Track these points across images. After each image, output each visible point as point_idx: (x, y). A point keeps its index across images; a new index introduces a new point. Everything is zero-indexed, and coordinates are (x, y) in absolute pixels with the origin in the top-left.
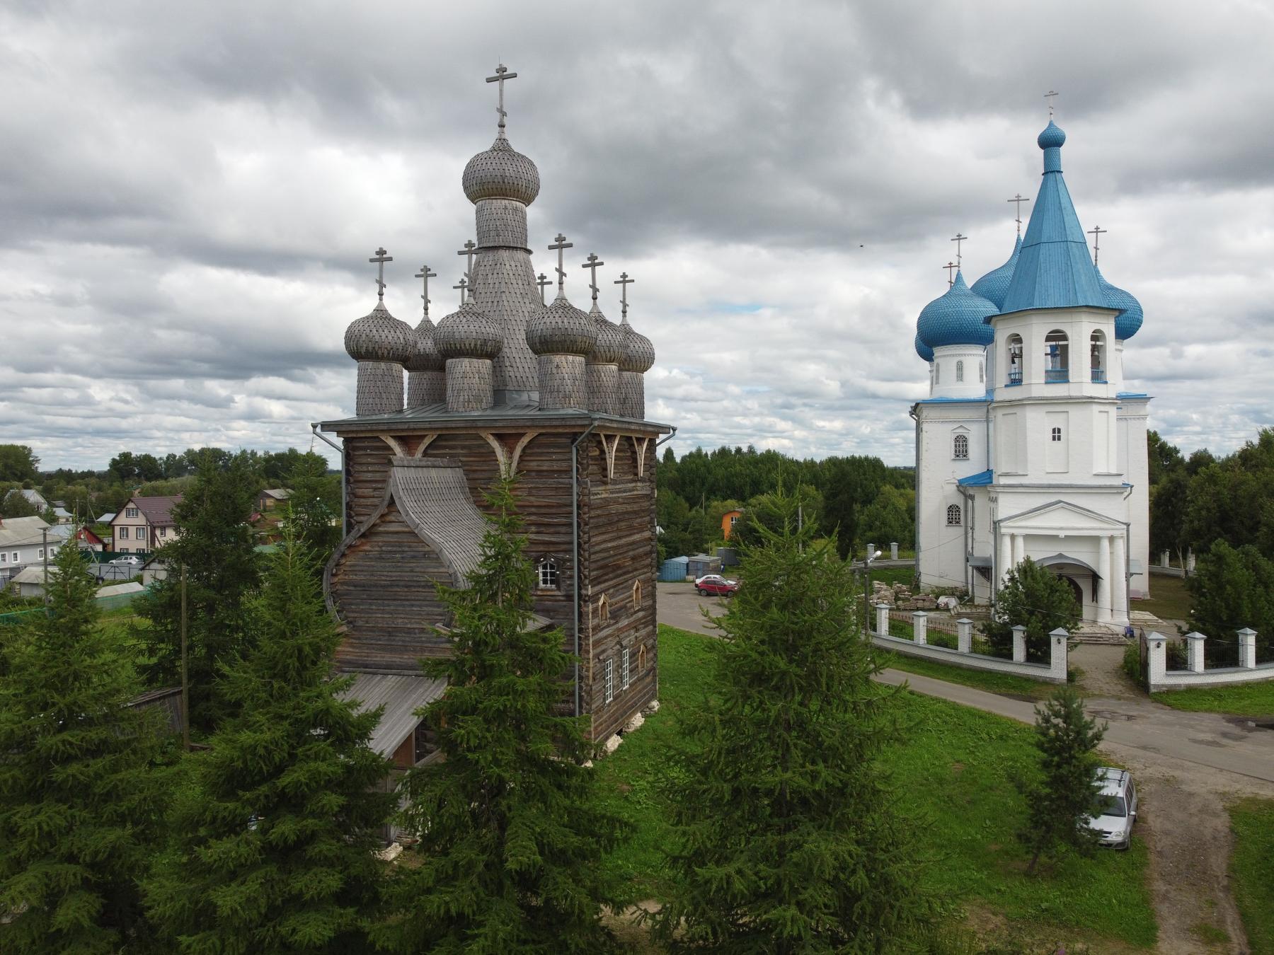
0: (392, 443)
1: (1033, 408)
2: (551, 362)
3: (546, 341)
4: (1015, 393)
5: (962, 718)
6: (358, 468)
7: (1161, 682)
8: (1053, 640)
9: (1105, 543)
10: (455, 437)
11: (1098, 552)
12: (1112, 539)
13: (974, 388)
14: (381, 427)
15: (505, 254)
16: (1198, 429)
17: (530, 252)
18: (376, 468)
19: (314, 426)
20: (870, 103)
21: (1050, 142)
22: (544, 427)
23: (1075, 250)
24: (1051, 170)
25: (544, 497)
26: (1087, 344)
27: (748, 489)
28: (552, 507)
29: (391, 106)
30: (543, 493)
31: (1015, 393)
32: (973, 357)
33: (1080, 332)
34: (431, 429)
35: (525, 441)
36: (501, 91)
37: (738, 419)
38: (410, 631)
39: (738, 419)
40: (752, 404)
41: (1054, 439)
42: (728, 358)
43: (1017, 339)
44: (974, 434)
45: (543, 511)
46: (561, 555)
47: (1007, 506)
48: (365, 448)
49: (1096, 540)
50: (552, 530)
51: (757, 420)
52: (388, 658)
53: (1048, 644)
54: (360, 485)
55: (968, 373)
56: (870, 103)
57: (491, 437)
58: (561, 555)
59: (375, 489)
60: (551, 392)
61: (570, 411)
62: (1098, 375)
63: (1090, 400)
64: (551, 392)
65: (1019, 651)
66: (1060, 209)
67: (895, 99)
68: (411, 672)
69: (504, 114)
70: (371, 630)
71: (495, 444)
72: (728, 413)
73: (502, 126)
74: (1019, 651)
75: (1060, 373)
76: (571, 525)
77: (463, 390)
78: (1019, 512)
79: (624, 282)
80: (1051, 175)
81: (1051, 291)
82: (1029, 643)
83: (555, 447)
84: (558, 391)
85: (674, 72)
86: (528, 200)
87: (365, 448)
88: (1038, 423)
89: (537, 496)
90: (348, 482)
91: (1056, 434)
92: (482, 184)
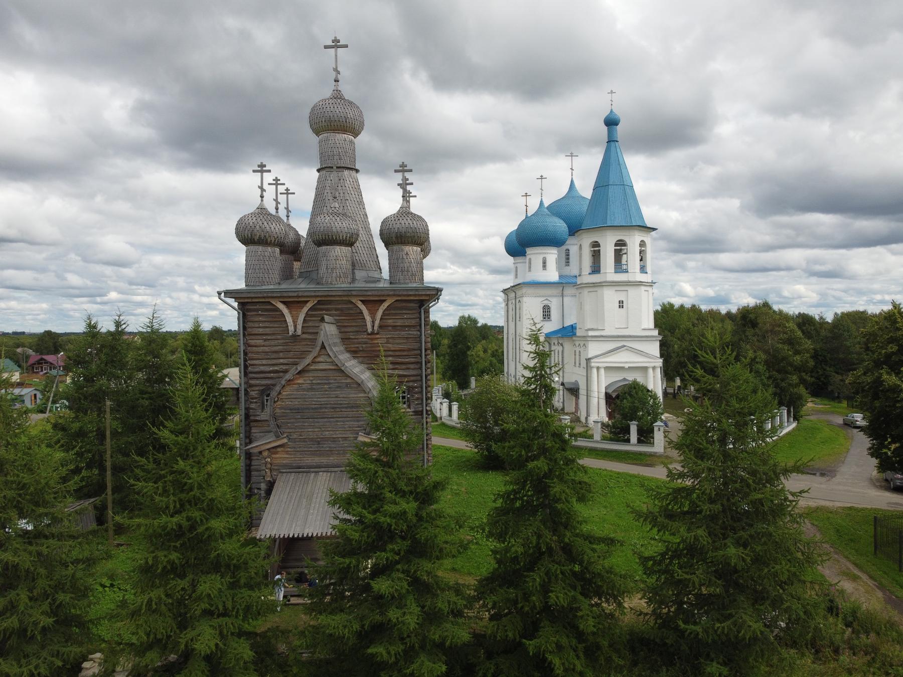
0: (281, 306)
2: (402, 250)
3: (401, 236)
4: (595, 278)
5: (628, 479)
6: (250, 324)
8: (656, 429)
9: (651, 371)
10: (330, 302)
11: (646, 377)
12: (654, 368)
13: (552, 275)
14: (275, 295)
15: (346, 172)
16: (27, 317)
17: (357, 171)
18: (267, 325)
19: (219, 293)
20: (407, 77)
22: (399, 296)
25: (398, 344)
26: (638, 249)
28: (404, 351)
29: (28, 34)
30: (397, 341)
31: (595, 278)
32: (552, 255)
33: (634, 240)
34: (388, 295)
35: (385, 305)
36: (336, 56)
38: (334, 440)
43: (596, 244)
44: (554, 304)
45: (397, 353)
46: (411, 384)
47: (594, 349)
48: (257, 310)
50: (404, 367)
52: (317, 460)
53: (652, 431)
54: (253, 337)
55: (546, 265)
56: (407, 77)
57: (360, 303)
58: (411, 384)
59: (265, 340)
60: (402, 271)
61: (415, 285)
62: (643, 269)
63: (640, 284)
64: (402, 271)
65: (634, 436)
66: (619, 164)
67: (423, 75)
68: (336, 469)
69: (339, 73)
70: (304, 440)
71: (363, 307)
73: (336, 81)
74: (634, 436)
75: (596, 269)
76: (421, 363)
77: (336, 268)
78: (600, 353)
79: (287, 194)
80: (612, 143)
81: (616, 217)
82: (640, 432)
83: (405, 309)
84: (408, 271)
85: (268, 37)
86: (356, 134)
87: (257, 310)
88: (610, 297)
89: (393, 344)
90: (244, 335)
91: (621, 304)
92: (330, 121)
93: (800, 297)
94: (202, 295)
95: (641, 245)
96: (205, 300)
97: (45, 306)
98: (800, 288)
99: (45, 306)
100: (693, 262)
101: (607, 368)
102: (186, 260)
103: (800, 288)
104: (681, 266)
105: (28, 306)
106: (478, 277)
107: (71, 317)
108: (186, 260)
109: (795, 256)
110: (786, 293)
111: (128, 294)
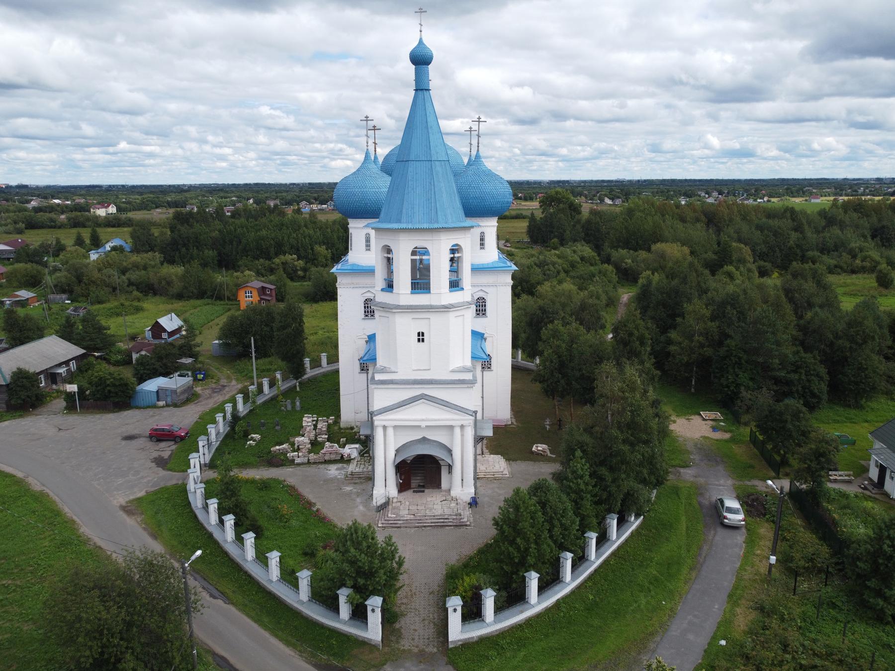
1: (402, 314)
7: (458, 638)
9: (457, 431)
12: (462, 427)
16: (37, 168)
21: (421, 60)
23: (439, 169)
24: (421, 88)
27: (272, 251)
37: (317, 145)
39: (317, 145)
40: (331, 135)
41: (419, 340)
42: (320, 98)
49: (451, 428)
51: (332, 146)
63: (447, 308)
66: (427, 128)
72: (311, 140)
74: (345, 611)
80: (420, 92)
88: (405, 327)
93: (829, 150)
94: (214, 146)
95: (453, 251)
96: (218, 151)
97: (54, 156)
98: (830, 140)
99: (54, 156)
100: (727, 111)
101: (395, 427)
102: (201, 108)
103: (830, 140)
104: (715, 118)
105: (38, 156)
106: (502, 127)
107: (79, 167)
108: (201, 108)
109: (836, 105)
110: (816, 146)
111: (139, 145)
